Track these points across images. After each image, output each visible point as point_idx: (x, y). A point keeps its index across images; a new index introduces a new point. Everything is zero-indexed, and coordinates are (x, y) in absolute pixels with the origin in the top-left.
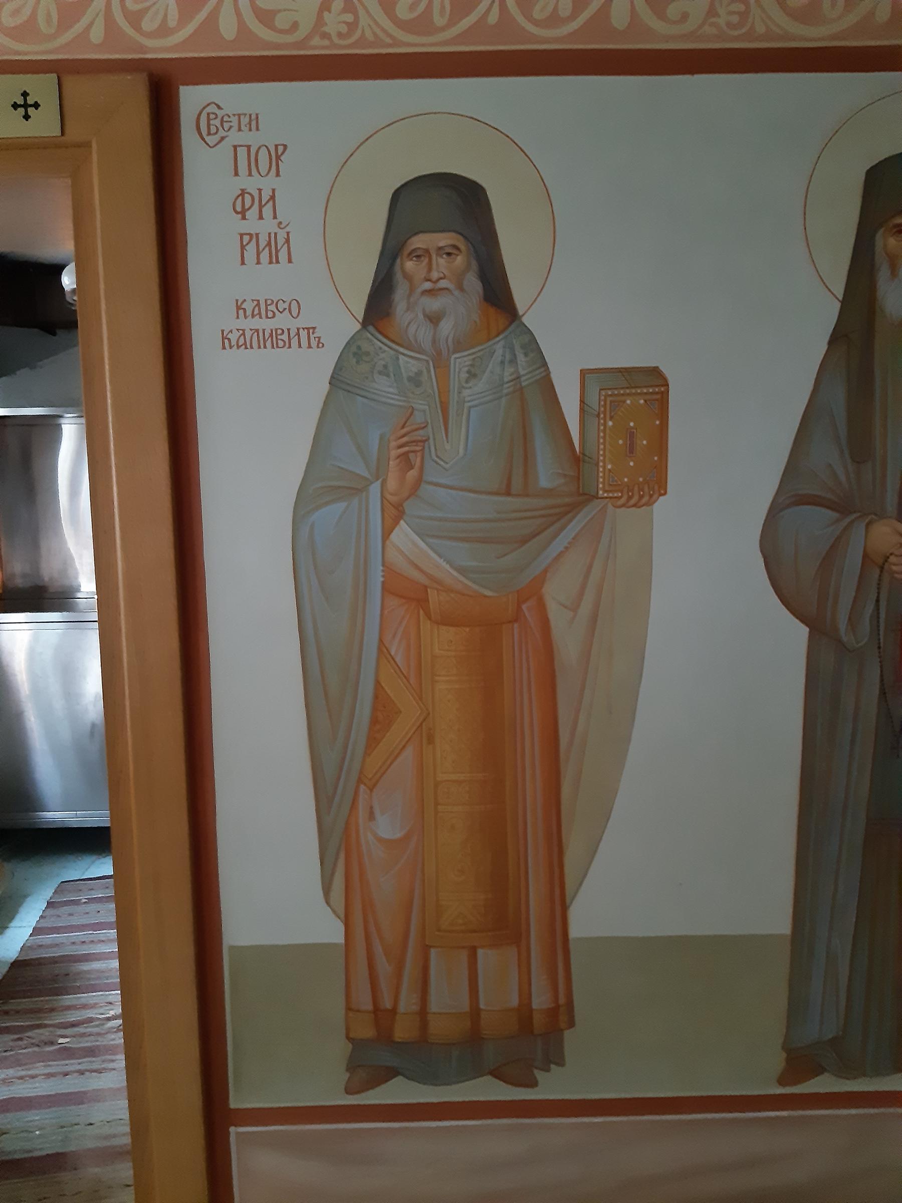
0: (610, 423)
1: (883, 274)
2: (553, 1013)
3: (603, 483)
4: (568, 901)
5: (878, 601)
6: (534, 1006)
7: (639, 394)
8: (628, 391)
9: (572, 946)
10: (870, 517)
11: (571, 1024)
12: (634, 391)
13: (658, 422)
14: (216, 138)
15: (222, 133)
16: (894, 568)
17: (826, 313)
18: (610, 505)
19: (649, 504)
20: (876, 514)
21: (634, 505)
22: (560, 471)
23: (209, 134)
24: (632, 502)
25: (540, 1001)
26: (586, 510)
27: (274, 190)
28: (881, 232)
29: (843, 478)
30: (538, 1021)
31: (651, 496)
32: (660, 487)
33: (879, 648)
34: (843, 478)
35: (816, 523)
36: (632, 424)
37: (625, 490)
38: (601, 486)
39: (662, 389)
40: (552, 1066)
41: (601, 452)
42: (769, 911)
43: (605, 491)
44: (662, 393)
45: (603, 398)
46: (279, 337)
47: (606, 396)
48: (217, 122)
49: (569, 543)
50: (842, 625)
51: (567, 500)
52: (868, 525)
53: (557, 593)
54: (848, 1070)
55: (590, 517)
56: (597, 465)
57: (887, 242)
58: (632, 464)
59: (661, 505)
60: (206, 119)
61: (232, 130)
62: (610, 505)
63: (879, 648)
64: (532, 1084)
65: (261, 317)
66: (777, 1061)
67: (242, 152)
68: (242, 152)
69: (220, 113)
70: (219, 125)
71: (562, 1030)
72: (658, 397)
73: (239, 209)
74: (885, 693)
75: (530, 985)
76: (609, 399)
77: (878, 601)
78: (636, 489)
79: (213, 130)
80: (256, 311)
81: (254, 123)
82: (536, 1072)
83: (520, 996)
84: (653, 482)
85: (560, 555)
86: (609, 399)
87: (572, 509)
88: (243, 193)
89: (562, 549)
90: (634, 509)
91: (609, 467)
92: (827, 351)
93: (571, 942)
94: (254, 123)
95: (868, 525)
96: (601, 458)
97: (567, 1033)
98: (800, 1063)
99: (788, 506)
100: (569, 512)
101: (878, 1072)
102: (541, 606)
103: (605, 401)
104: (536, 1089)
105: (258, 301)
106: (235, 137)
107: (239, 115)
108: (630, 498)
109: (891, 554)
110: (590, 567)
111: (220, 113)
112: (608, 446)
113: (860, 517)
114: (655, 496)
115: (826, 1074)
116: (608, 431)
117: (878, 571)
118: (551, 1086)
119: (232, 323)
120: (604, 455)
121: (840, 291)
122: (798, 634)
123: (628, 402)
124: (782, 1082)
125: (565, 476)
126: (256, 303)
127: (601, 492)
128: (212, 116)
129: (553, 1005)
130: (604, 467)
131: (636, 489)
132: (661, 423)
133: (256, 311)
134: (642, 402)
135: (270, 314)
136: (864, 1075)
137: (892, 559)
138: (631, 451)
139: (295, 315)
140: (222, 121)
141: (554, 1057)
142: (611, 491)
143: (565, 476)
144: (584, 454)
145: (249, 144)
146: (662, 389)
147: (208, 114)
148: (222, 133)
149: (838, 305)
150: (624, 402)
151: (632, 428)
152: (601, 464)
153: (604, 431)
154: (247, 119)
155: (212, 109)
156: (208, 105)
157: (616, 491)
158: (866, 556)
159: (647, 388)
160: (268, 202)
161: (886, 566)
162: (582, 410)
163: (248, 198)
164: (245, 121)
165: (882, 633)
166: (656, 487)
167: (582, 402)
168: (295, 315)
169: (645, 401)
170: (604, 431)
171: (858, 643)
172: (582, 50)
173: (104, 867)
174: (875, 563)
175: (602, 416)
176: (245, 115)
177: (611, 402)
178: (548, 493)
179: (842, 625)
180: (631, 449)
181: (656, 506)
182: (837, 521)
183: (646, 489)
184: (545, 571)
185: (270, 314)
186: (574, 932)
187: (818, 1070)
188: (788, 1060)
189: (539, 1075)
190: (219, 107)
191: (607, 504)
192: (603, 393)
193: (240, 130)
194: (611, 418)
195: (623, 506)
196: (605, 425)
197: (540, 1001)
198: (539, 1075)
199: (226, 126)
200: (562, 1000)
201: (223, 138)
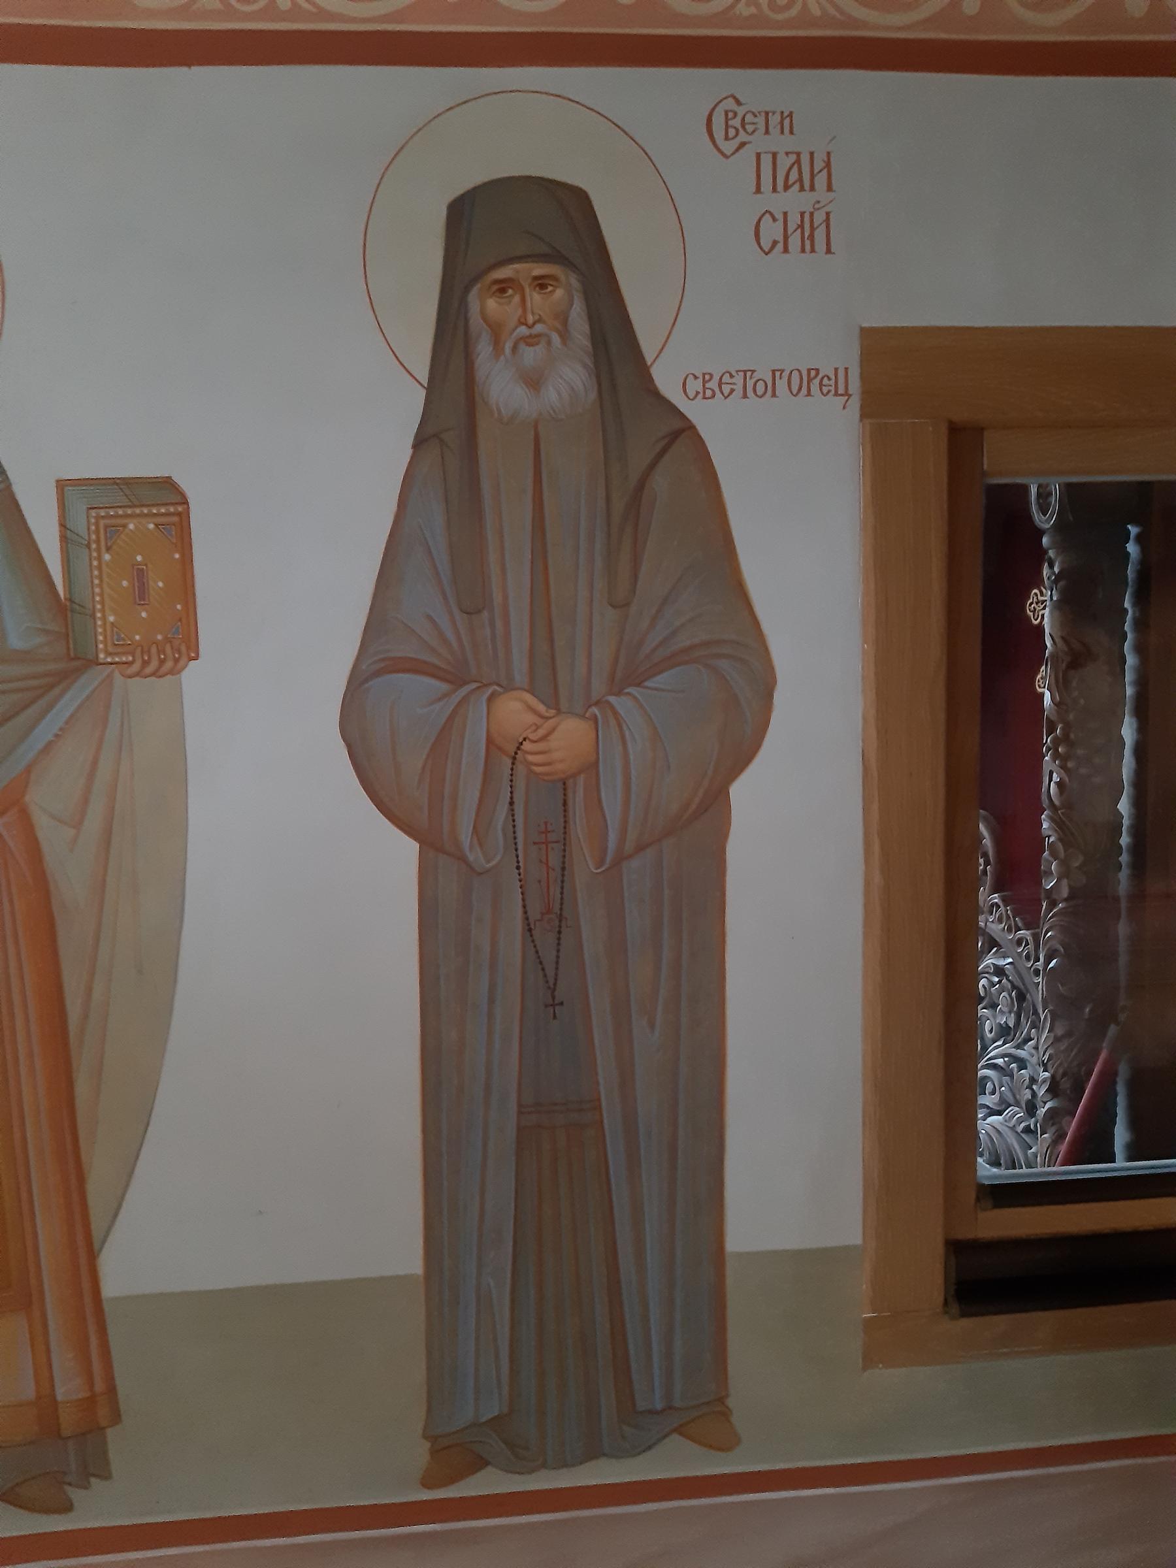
0: (107, 557)
1: (483, 349)
2: (89, 1403)
3: (105, 642)
4: (96, 1246)
5: (511, 803)
6: (59, 1398)
7: (146, 515)
8: (129, 511)
9: (107, 1307)
10: (490, 690)
11: (116, 1417)
12: (138, 511)
13: (177, 556)
14: (734, 144)
15: (743, 137)
16: (530, 758)
17: (408, 405)
18: (117, 675)
19: (175, 671)
20: (499, 685)
21: (153, 674)
22: (39, 626)
23: (727, 138)
24: (149, 669)
25: (68, 1389)
26: (83, 679)
28: (475, 291)
29: (450, 635)
30: (68, 1420)
31: (176, 661)
32: (188, 648)
33: (518, 868)
34: (450, 635)
35: (415, 698)
36: (139, 558)
37: (139, 650)
38: (101, 646)
39: (180, 509)
40: (93, 1480)
41: (98, 598)
42: (394, 1244)
43: (109, 654)
44: (179, 514)
45: (93, 520)
47: (98, 518)
48: (737, 123)
49: (61, 729)
50: (465, 836)
51: (52, 667)
52: (490, 699)
53: (48, 800)
54: (521, 1457)
55: (87, 692)
56: (93, 616)
57: (484, 306)
58: (144, 615)
59: (192, 676)
62: (117, 675)
63: (518, 868)
64: (66, 1507)
66: (419, 1454)
67: (766, 161)
68: (766, 161)
69: (741, 111)
70: (739, 126)
71: (104, 1428)
72: (175, 519)
74: (530, 930)
75: (50, 1366)
76: (102, 523)
77: (511, 803)
78: (154, 650)
79: (732, 132)
80: (794, 176)
81: (787, 122)
82: (67, 1487)
83: (37, 1382)
84: (177, 642)
85: (48, 747)
86: (102, 523)
87: (64, 678)
89: (50, 737)
90: (153, 678)
91: (112, 619)
92: (412, 458)
93: (104, 1303)
95: (490, 699)
96: (99, 607)
97: (110, 1433)
98: (453, 1454)
99: (377, 674)
100: (52, 687)
101: (564, 1464)
102: (25, 817)
103: (97, 524)
104: (71, 1515)
105: (798, 154)
106: (759, 142)
108: (145, 663)
109: (525, 739)
110: (95, 763)
111: (741, 111)
112: (107, 590)
113: (478, 688)
114: (182, 663)
115: (489, 1469)
116: (104, 567)
117: (509, 761)
118: (94, 1509)
120: (102, 603)
121: (424, 375)
122: (403, 852)
123: (131, 526)
124: (428, 1482)
125: (47, 632)
126: (793, 158)
127: (102, 656)
128: (730, 115)
129: (88, 1394)
130: (104, 618)
131: (154, 650)
132: (183, 555)
133: (794, 176)
134: (151, 526)
135: (709, 393)
136: (544, 1466)
137: (527, 746)
138: (142, 598)
139: (795, 392)
141: (95, 1467)
142: (116, 654)
143: (47, 632)
144: (71, 600)
145: (774, 150)
146: (180, 509)
147: (726, 113)
148: (743, 137)
149: (422, 393)
150: (125, 526)
151: (139, 564)
152: (99, 615)
153: (99, 568)
154: (778, 117)
155: (730, 104)
157: (125, 653)
158: (490, 741)
159: (159, 505)
161: (520, 755)
162: (64, 539)
164: (774, 120)
165: (520, 847)
166: (183, 648)
167: (63, 525)
168: (795, 392)
169: (156, 525)
170: (99, 568)
171: (488, 862)
172: (833, 38)
173: (986, 1171)
174: (505, 754)
175: (94, 546)
177: (106, 527)
178: (23, 657)
179: (465, 836)
180: (141, 593)
181: (185, 675)
182: (446, 695)
183: (183, 648)
184: (28, 770)
185: (709, 393)
186: (110, 1288)
187: (479, 1463)
188: (434, 1453)
189: (75, 1494)
190: (738, 103)
191: (112, 672)
192: (93, 513)
194: (108, 549)
195: (137, 674)
196: (99, 558)
197: (68, 1389)
198: (75, 1494)
200: (99, 1386)
201: (743, 144)
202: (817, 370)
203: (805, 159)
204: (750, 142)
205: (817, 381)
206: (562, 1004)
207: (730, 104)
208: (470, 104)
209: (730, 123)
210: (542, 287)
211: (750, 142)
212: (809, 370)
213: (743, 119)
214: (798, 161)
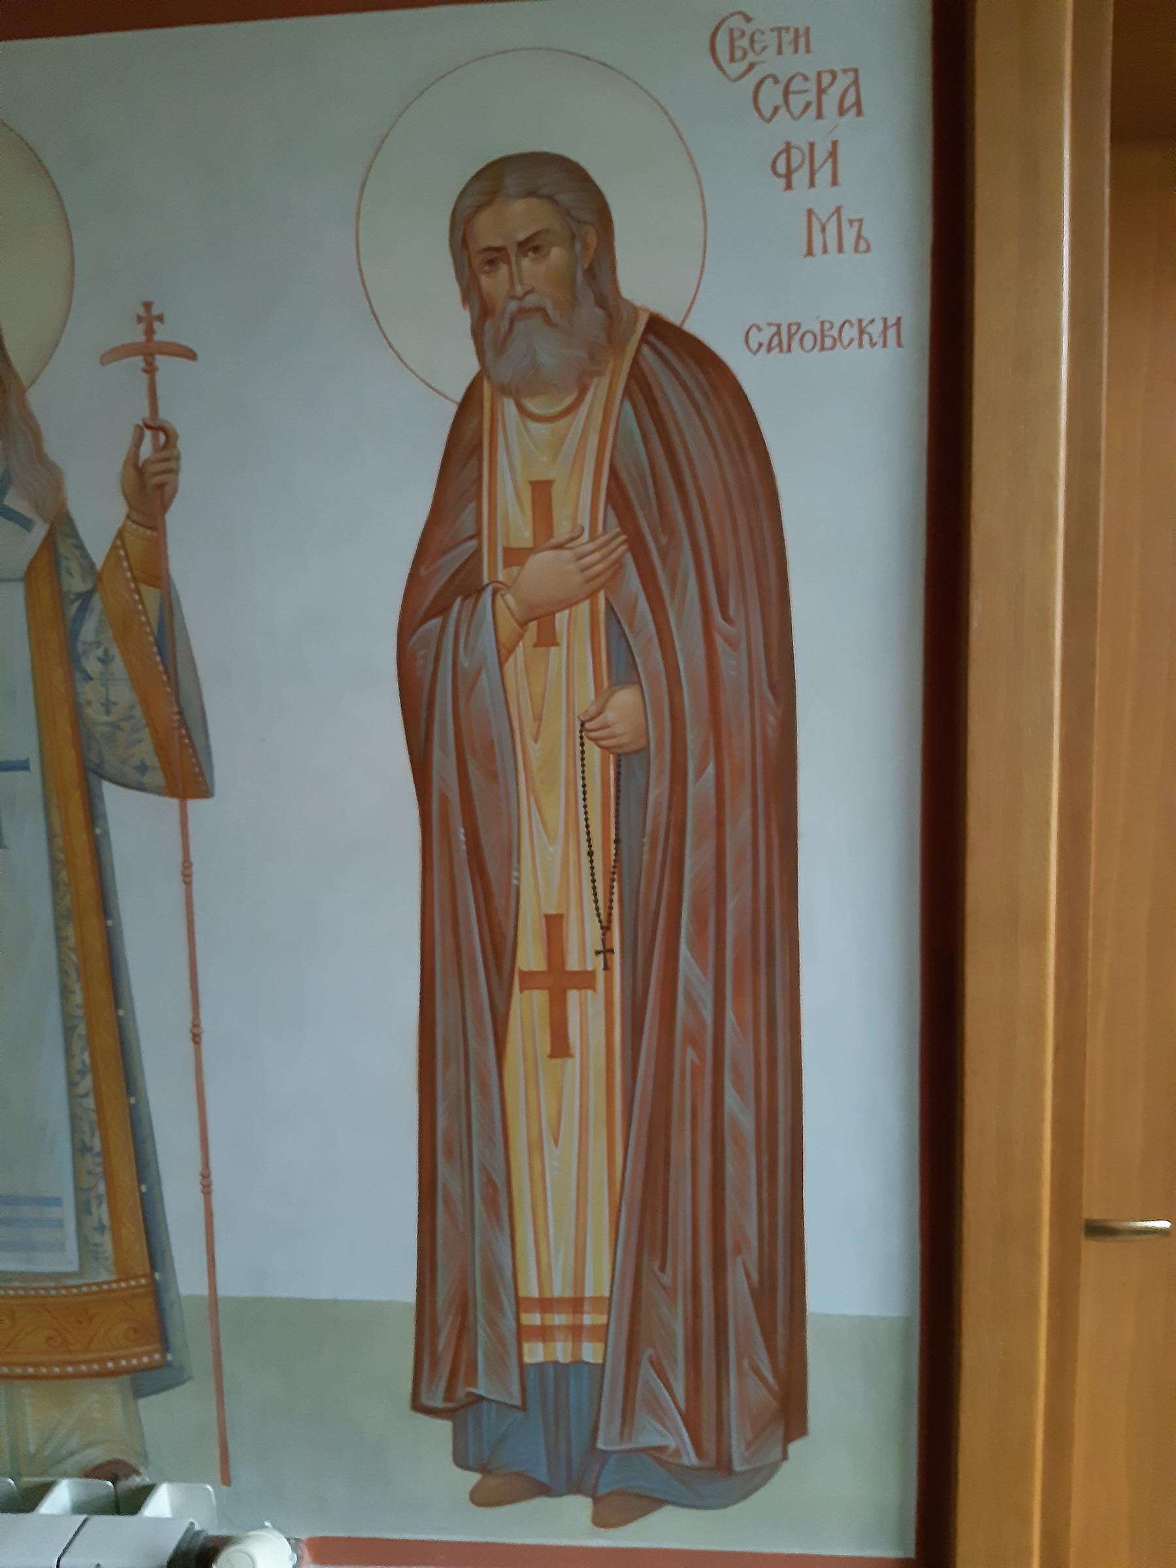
15: (751, 57)
23: (732, 59)
27: (835, 144)
46: (826, 333)
48: (744, 42)
60: (727, 40)
61: (767, 51)
65: (781, 350)
69: (749, 28)
73: (781, 167)
79: (738, 54)
80: (775, 342)
81: (802, 40)
88: (788, 148)
94: (892, 332)
105: (779, 326)
107: (779, 30)
119: (52, 1212)
126: (774, 329)
129: (600, 1361)
133: (775, 342)
140: (752, 41)
147: (731, 31)
148: (751, 57)
154: (791, 36)
155: (736, 22)
156: (732, 15)
160: (825, 162)
163: (795, 154)
164: (788, 37)
176: (787, 29)
190: (748, 19)
193: (780, 52)
199: (758, 47)
201: (752, 66)
202: (799, 325)
203: (784, 330)
204: (758, 63)
205: (797, 337)
206: (598, 953)
207: (736, 22)
208: (362, 210)
209: (737, 43)
210: (491, 262)
211: (758, 63)
212: (789, 326)
213: (752, 36)
214: (778, 333)
